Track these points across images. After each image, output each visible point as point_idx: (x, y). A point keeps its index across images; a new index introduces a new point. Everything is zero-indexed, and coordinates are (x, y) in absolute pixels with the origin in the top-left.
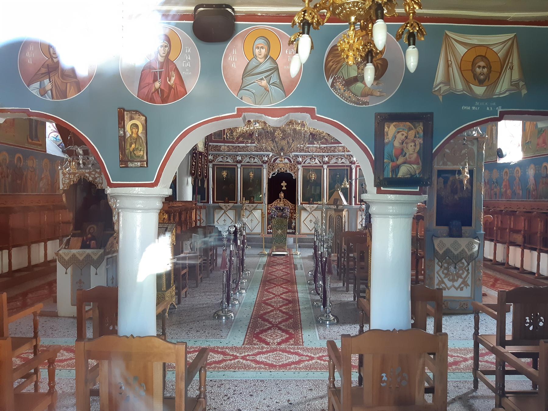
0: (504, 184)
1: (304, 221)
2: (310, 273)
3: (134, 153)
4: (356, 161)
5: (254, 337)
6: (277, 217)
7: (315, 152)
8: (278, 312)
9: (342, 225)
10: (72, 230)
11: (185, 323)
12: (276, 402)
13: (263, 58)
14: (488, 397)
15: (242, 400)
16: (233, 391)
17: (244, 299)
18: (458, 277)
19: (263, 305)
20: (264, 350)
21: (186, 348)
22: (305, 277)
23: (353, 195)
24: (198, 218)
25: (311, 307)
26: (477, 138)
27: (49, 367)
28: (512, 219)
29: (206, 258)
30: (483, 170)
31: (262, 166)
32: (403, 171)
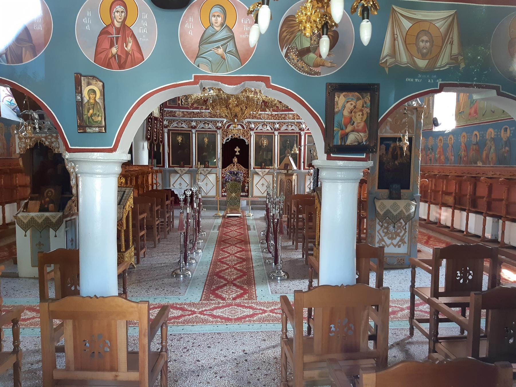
0: (438, 150)
1: (257, 184)
2: (262, 233)
3: (92, 119)
4: (305, 128)
5: (211, 293)
6: (231, 181)
7: (267, 119)
8: (232, 270)
9: (292, 189)
10: (30, 193)
11: (144, 281)
12: (233, 353)
13: (219, 26)
14: (423, 343)
15: (201, 352)
16: (192, 344)
17: (200, 258)
18: (396, 236)
19: (219, 263)
20: (221, 305)
21: (149, 306)
22: (258, 237)
23: (302, 160)
24: (154, 182)
25: (264, 264)
26: (417, 108)
27: (13, 327)
28: (445, 182)
29: (163, 220)
30: (421, 138)
31: (216, 131)
32: (351, 139)
